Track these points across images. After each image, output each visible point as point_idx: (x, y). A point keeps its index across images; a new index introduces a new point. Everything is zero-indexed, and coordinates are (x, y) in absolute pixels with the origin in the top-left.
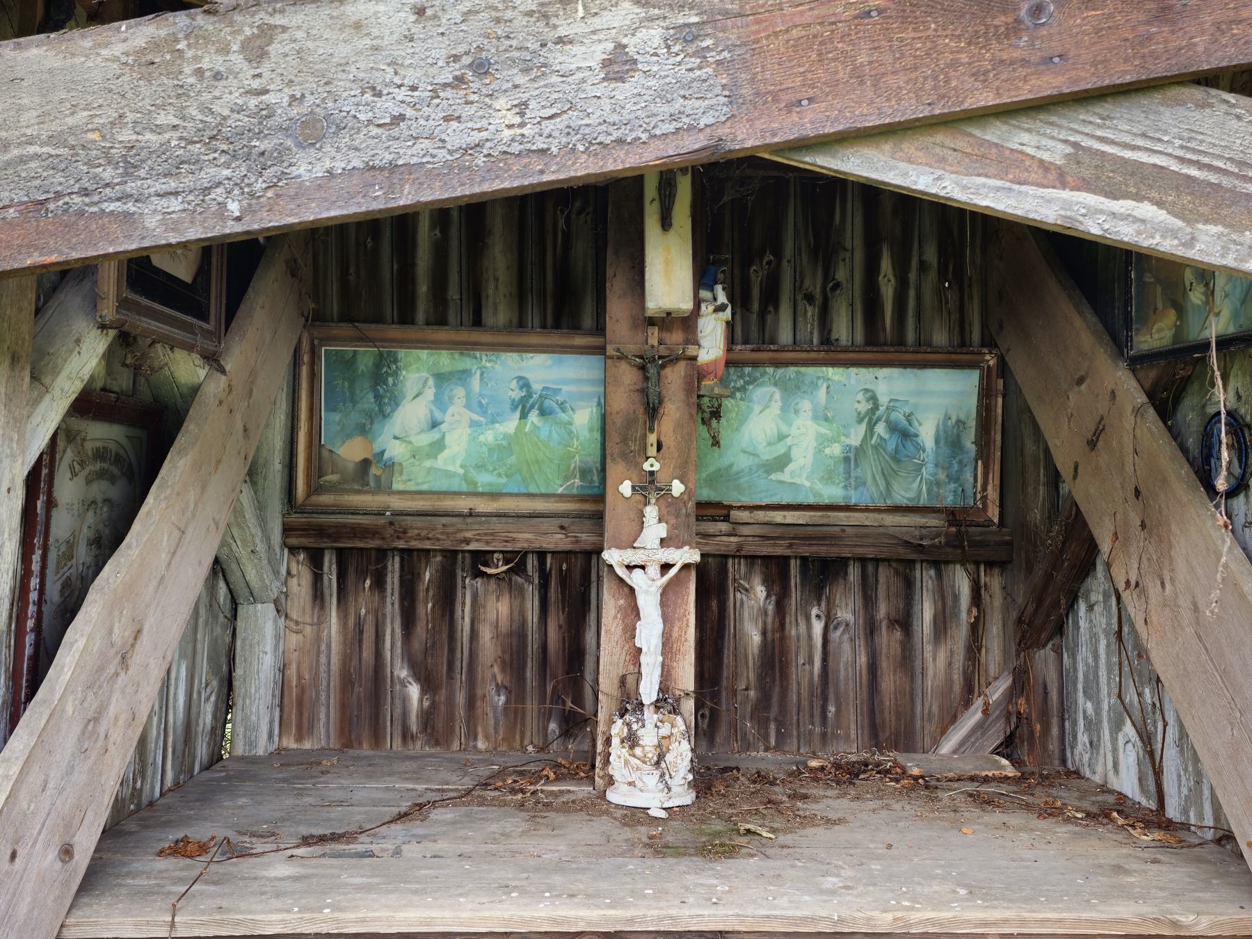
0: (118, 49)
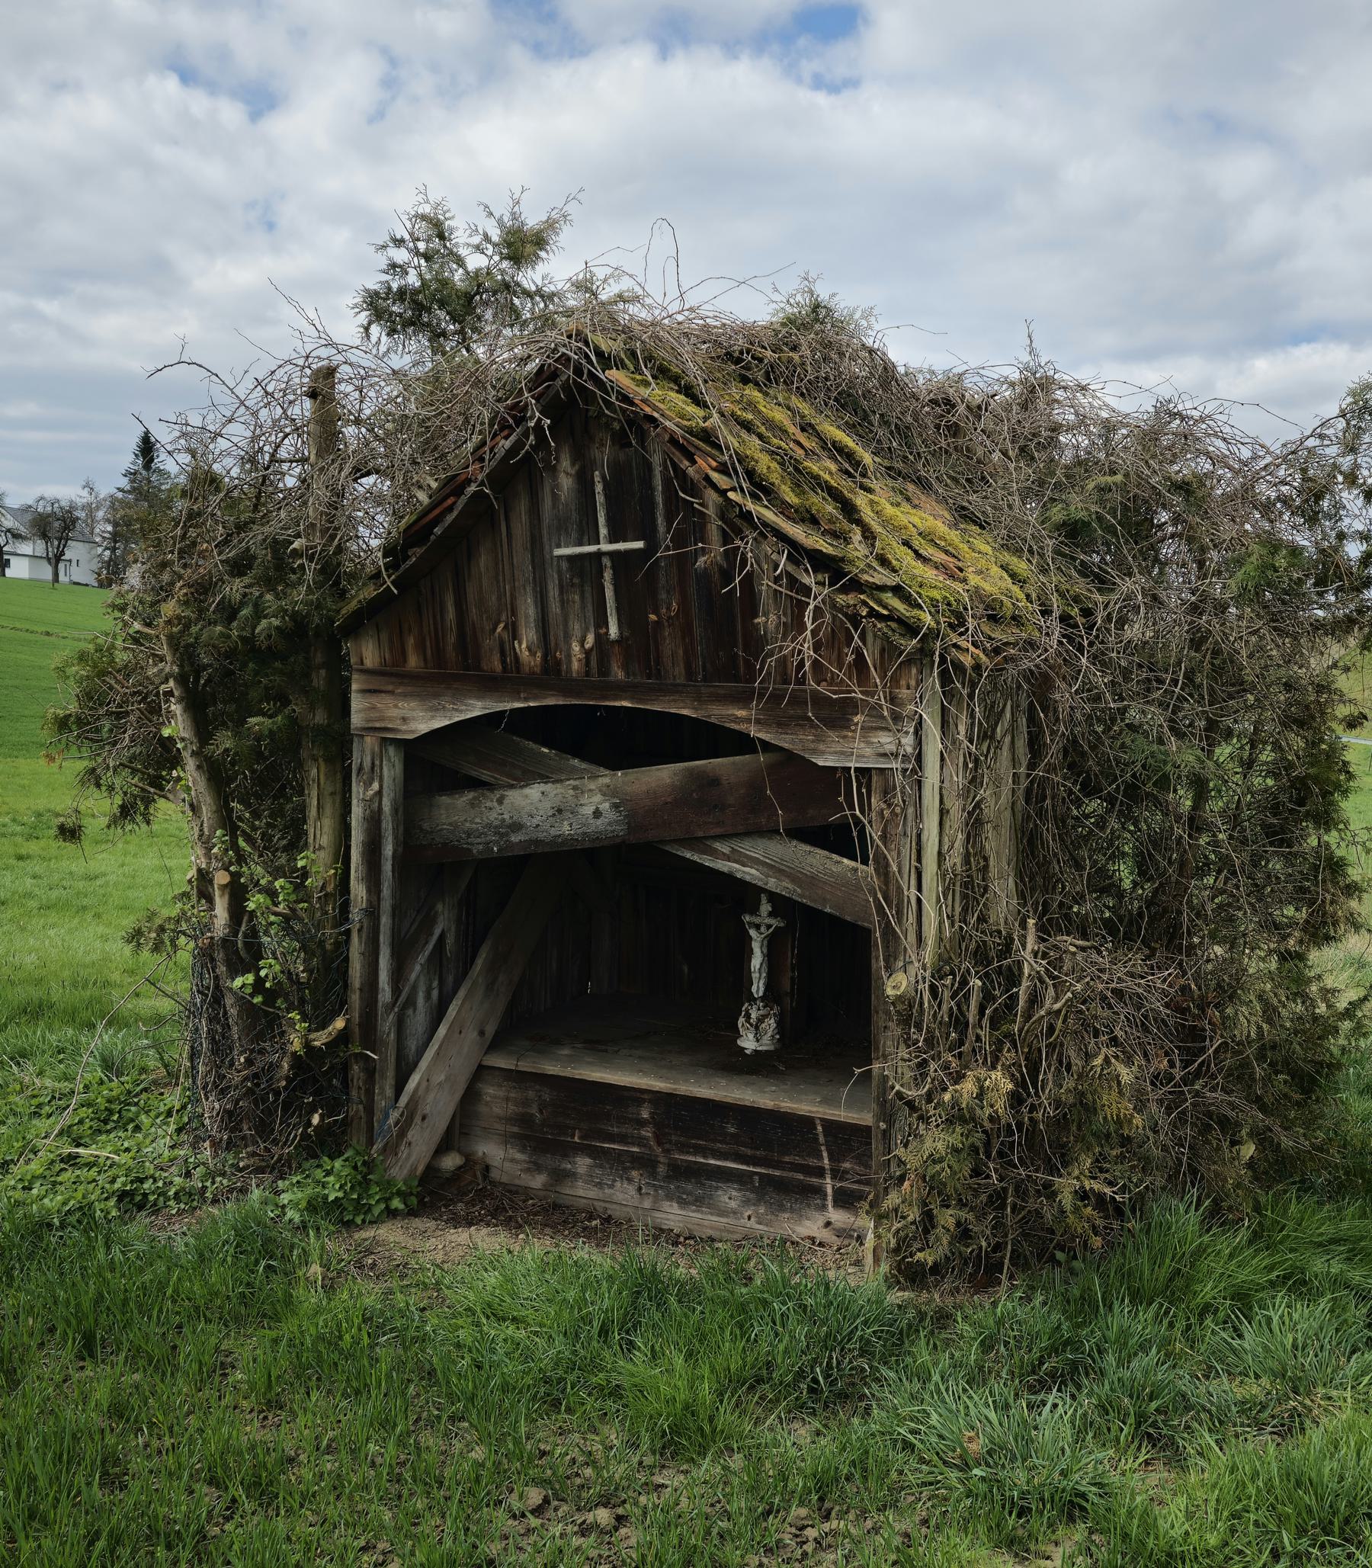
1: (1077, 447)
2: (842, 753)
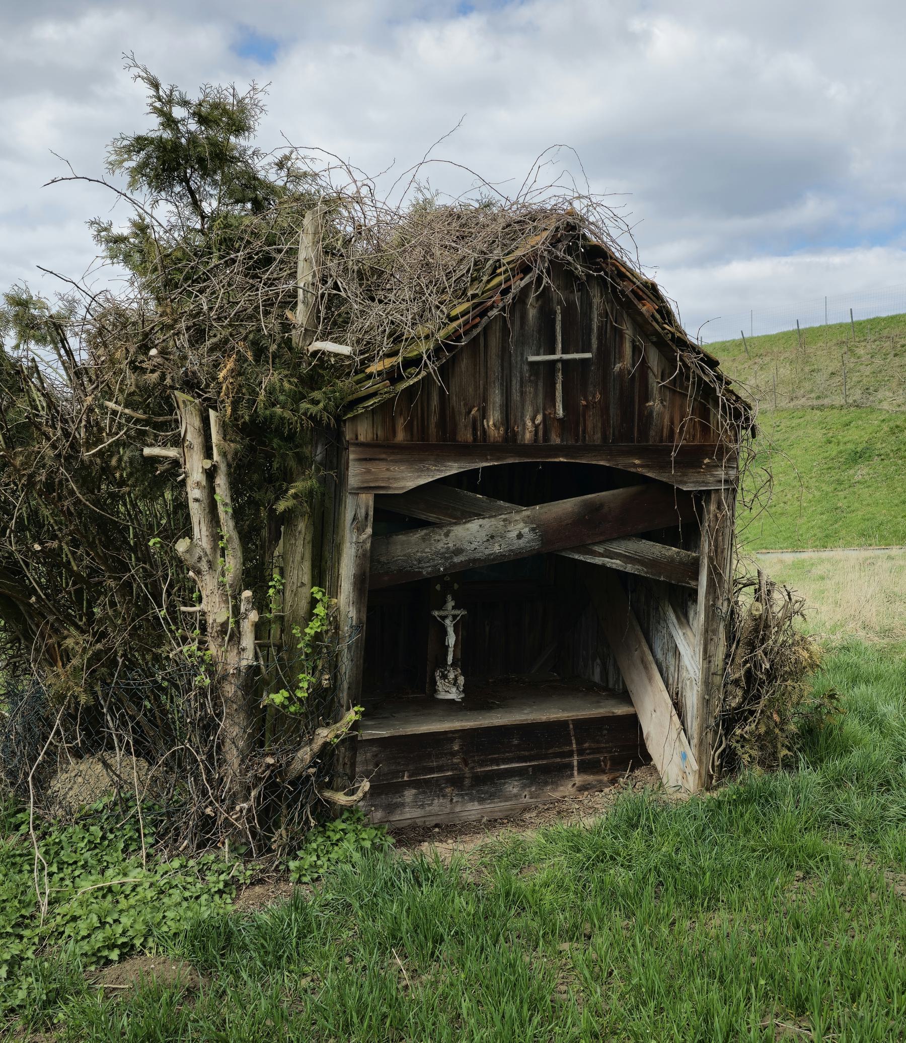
0: (418, 536)
1: (353, 324)
2: (697, 482)
